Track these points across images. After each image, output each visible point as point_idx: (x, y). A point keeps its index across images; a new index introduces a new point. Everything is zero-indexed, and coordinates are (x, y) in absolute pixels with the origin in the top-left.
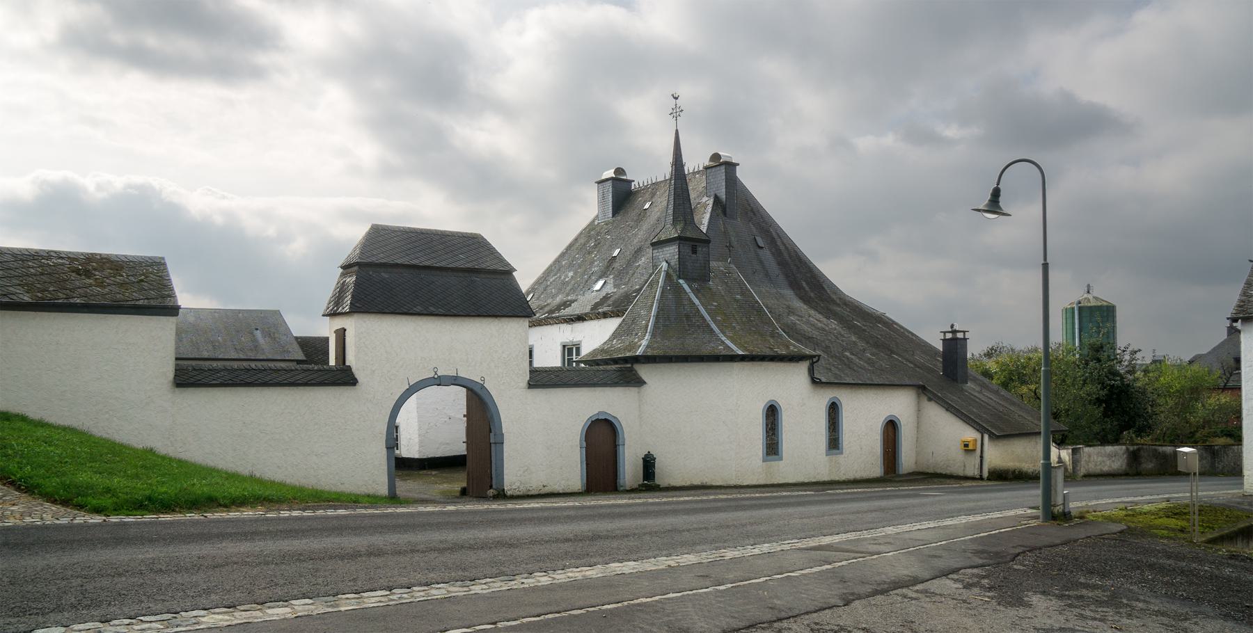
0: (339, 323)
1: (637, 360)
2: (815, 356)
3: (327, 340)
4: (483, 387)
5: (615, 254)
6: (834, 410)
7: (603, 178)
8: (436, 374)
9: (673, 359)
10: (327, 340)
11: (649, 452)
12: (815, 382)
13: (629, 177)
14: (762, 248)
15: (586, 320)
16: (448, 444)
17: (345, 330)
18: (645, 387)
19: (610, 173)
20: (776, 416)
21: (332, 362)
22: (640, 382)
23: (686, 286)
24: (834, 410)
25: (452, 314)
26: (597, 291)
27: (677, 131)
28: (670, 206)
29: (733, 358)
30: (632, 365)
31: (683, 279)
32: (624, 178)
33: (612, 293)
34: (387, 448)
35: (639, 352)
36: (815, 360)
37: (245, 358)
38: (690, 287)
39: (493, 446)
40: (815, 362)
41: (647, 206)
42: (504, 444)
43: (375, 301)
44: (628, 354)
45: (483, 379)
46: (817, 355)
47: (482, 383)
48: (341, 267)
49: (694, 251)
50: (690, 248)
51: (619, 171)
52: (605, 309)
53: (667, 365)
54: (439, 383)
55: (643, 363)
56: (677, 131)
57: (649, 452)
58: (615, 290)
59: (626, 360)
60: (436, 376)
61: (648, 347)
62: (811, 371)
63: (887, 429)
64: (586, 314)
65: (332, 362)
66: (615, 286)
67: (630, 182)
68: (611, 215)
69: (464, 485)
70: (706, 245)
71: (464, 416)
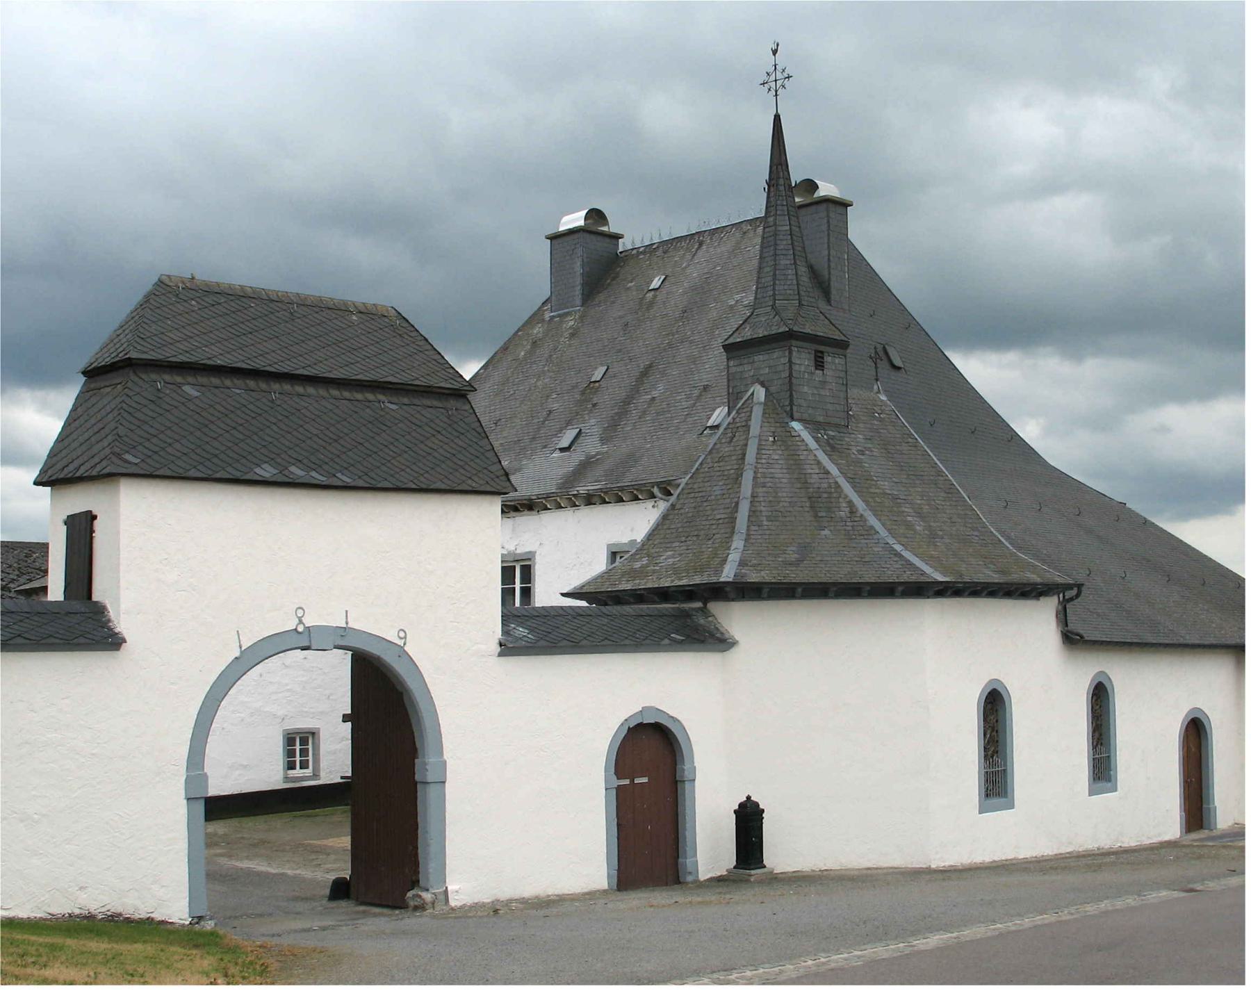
0: (78, 501)
1: (718, 592)
2: (1069, 587)
3: (43, 548)
4: (402, 653)
5: (597, 375)
6: (1100, 696)
7: (561, 229)
8: (301, 622)
9: (766, 591)
10: (43, 548)
11: (749, 798)
12: (1072, 639)
13: (613, 228)
14: (899, 368)
15: (546, 509)
16: (245, 767)
17: (95, 517)
18: (733, 654)
19: (575, 219)
20: (1000, 713)
21: (56, 589)
22: (718, 641)
23: (806, 435)
24: (1100, 696)
25: (340, 483)
26: (562, 450)
27: (777, 119)
28: (784, 262)
29: (919, 590)
30: (705, 604)
31: (799, 420)
32: (605, 229)
33: (598, 454)
34: (188, 799)
35: (728, 574)
36: (1069, 594)
37: (996, 578)
38: (817, 440)
39: (419, 786)
40: (1071, 599)
41: (656, 283)
42: (446, 784)
43: (169, 450)
44: (697, 580)
45: (402, 634)
46: (1075, 585)
47: (401, 643)
48: (85, 373)
49: (819, 364)
50: (813, 356)
51: (596, 215)
52: (592, 487)
53: (783, 604)
54: (306, 644)
55: (733, 600)
56: (777, 119)
57: (749, 798)
58: (605, 449)
59: (689, 593)
60: (301, 629)
61: (742, 563)
62: (1063, 617)
63: (1187, 737)
64: (547, 497)
65: (56, 589)
66: (604, 440)
67: (617, 237)
68: (578, 302)
69: (347, 874)
70: (840, 351)
71: (346, 718)
